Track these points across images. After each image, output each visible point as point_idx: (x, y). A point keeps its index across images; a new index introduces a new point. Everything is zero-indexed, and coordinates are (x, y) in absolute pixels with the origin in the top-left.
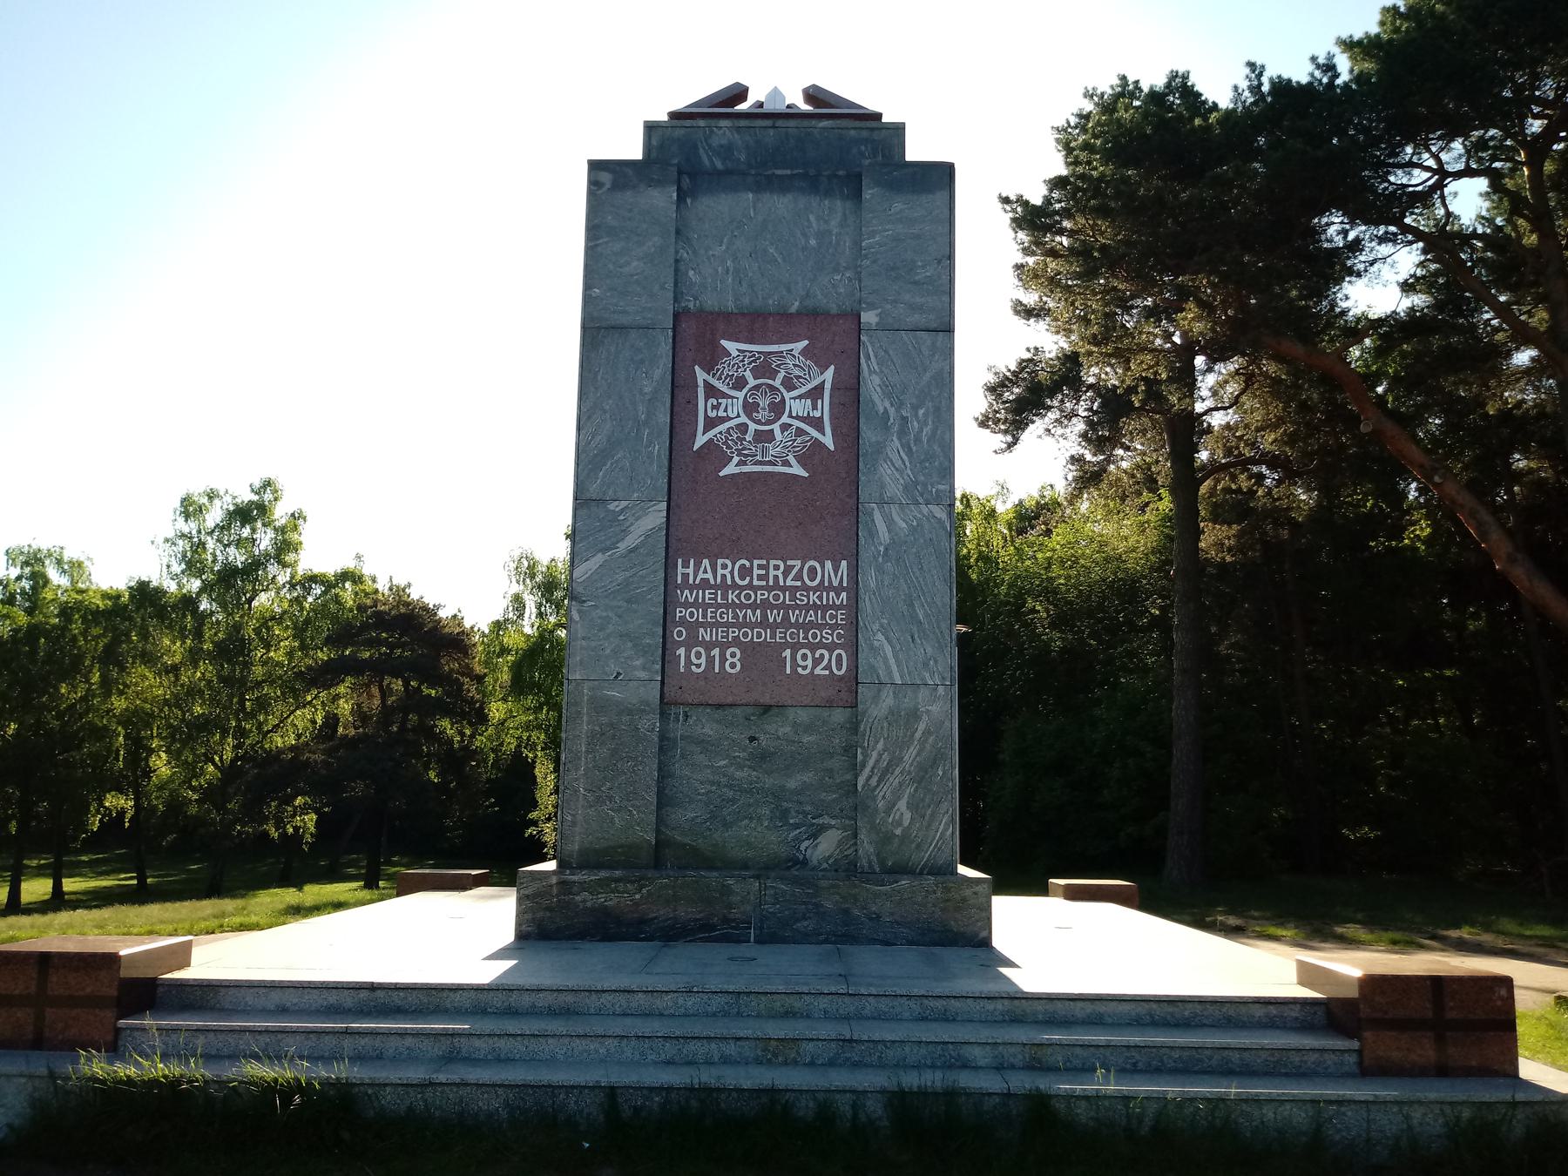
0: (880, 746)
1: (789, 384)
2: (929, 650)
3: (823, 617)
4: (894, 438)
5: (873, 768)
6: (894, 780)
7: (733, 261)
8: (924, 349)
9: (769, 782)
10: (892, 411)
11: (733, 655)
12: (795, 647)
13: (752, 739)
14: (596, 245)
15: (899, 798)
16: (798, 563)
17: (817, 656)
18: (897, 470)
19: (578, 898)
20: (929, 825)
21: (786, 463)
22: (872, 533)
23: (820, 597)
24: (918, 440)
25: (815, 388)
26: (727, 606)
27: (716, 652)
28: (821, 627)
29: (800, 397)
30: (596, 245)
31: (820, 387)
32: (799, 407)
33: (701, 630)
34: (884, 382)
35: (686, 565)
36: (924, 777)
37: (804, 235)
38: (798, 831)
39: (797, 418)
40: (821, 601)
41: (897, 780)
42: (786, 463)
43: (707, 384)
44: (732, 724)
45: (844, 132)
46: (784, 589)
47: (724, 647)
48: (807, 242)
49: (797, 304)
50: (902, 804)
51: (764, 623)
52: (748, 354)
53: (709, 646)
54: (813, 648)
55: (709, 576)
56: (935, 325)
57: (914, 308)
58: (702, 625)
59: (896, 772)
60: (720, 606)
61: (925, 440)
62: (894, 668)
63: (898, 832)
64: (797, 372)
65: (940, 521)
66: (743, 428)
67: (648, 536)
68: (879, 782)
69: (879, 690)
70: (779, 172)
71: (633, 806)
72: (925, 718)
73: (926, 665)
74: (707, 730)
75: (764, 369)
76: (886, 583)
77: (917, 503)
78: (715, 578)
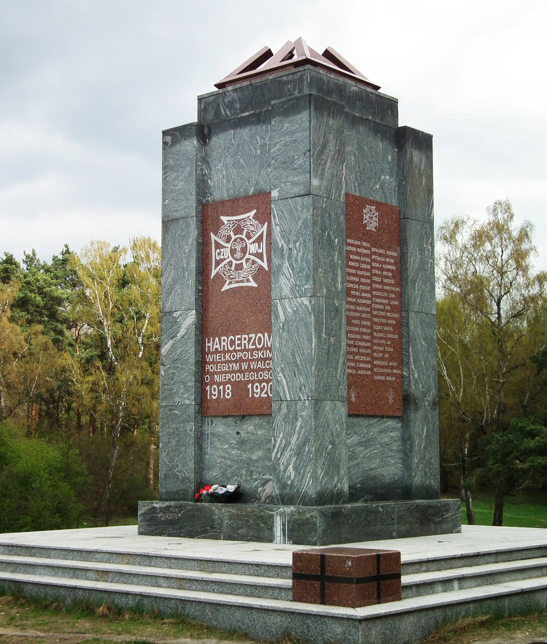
0: (281, 436)
1: (249, 237)
2: (302, 380)
3: (264, 365)
4: (286, 262)
5: (278, 448)
6: (287, 454)
7: (226, 171)
8: (298, 207)
9: (245, 456)
10: (285, 245)
11: (228, 389)
12: (253, 382)
13: (238, 433)
14: (166, 177)
15: (289, 464)
16: (253, 335)
17: (262, 386)
18: (287, 279)
19: (159, 515)
20: (302, 479)
21: (248, 281)
22: (277, 317)
23: (263, 354)
24: (296, 260)
25: (259, 237)
26: (225, 362)
27: (221, 387)
28: (263, 370)
29: (253, 242)
30: (166, 177)
31: (262, 233)
32: (253, 248)
33: (216, 376)
34: (281, 230)
35: (209, 342)
36: (300, 452)
37: (255, 149)
38: (257, 482)
39: (252, 254)
40: (263, 356)
41: (288, 454)
42: (248, 281)
43: (216, 242)
44: (230, 426)
45: (281, 79)
46: (248, 351)
47: (224, 384)
48: (256, 152)
49: (252, 189)
50: (291, 467)
51: (240, 371)
52: (232, 222)
53: (219, 384)
54: (260, 382)
55: (218, 346)
56: (303, 192)
57: (294, 184)
58: (216, 373)
59: (288, 450)
60: (222, 362)
61: (299, 260)
62: (287, 392)
63: (289, 482)
64: (252, 228)
65: (306, 306)
66: (230, 263)
67: (188, 329)
68: (281, 455)
69: (281, 405)
70: (244, 115)
71: (185, 470)
72: (300, 419)
73: (301, 389)
74: (220, 430)
75: (238, 230)
76: (283, 344)
77: (296, 297)
78: (221, 347)
